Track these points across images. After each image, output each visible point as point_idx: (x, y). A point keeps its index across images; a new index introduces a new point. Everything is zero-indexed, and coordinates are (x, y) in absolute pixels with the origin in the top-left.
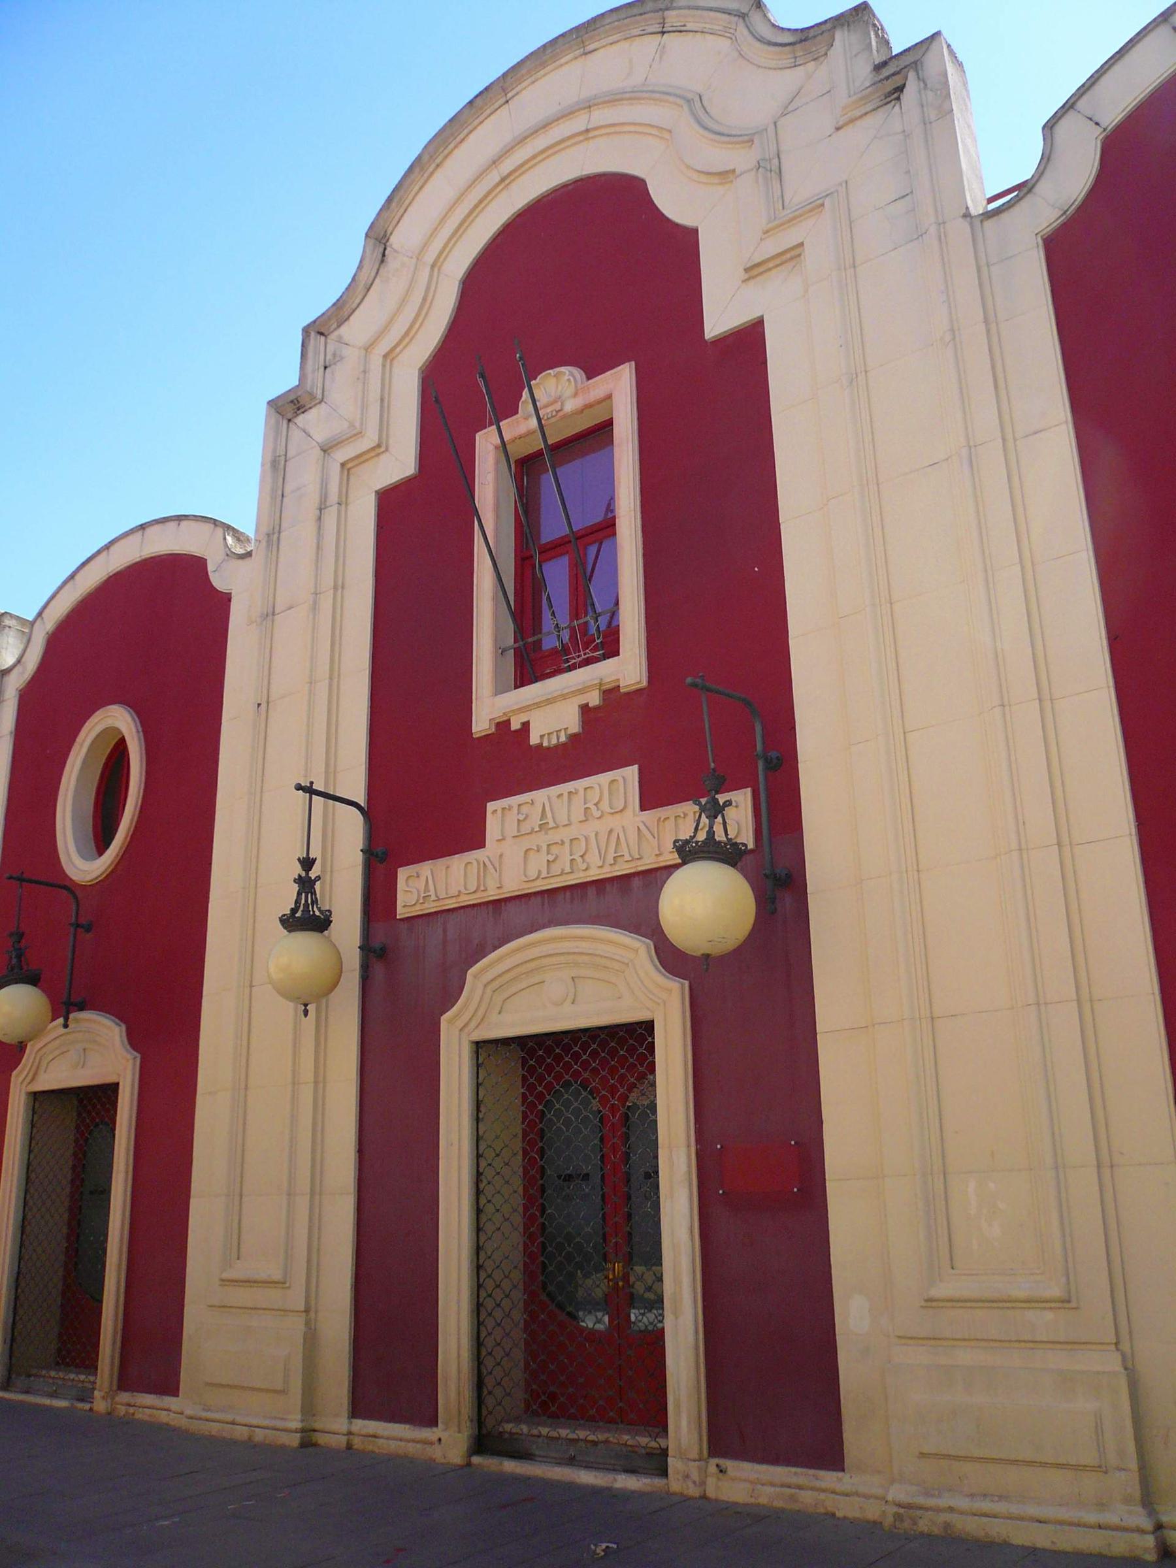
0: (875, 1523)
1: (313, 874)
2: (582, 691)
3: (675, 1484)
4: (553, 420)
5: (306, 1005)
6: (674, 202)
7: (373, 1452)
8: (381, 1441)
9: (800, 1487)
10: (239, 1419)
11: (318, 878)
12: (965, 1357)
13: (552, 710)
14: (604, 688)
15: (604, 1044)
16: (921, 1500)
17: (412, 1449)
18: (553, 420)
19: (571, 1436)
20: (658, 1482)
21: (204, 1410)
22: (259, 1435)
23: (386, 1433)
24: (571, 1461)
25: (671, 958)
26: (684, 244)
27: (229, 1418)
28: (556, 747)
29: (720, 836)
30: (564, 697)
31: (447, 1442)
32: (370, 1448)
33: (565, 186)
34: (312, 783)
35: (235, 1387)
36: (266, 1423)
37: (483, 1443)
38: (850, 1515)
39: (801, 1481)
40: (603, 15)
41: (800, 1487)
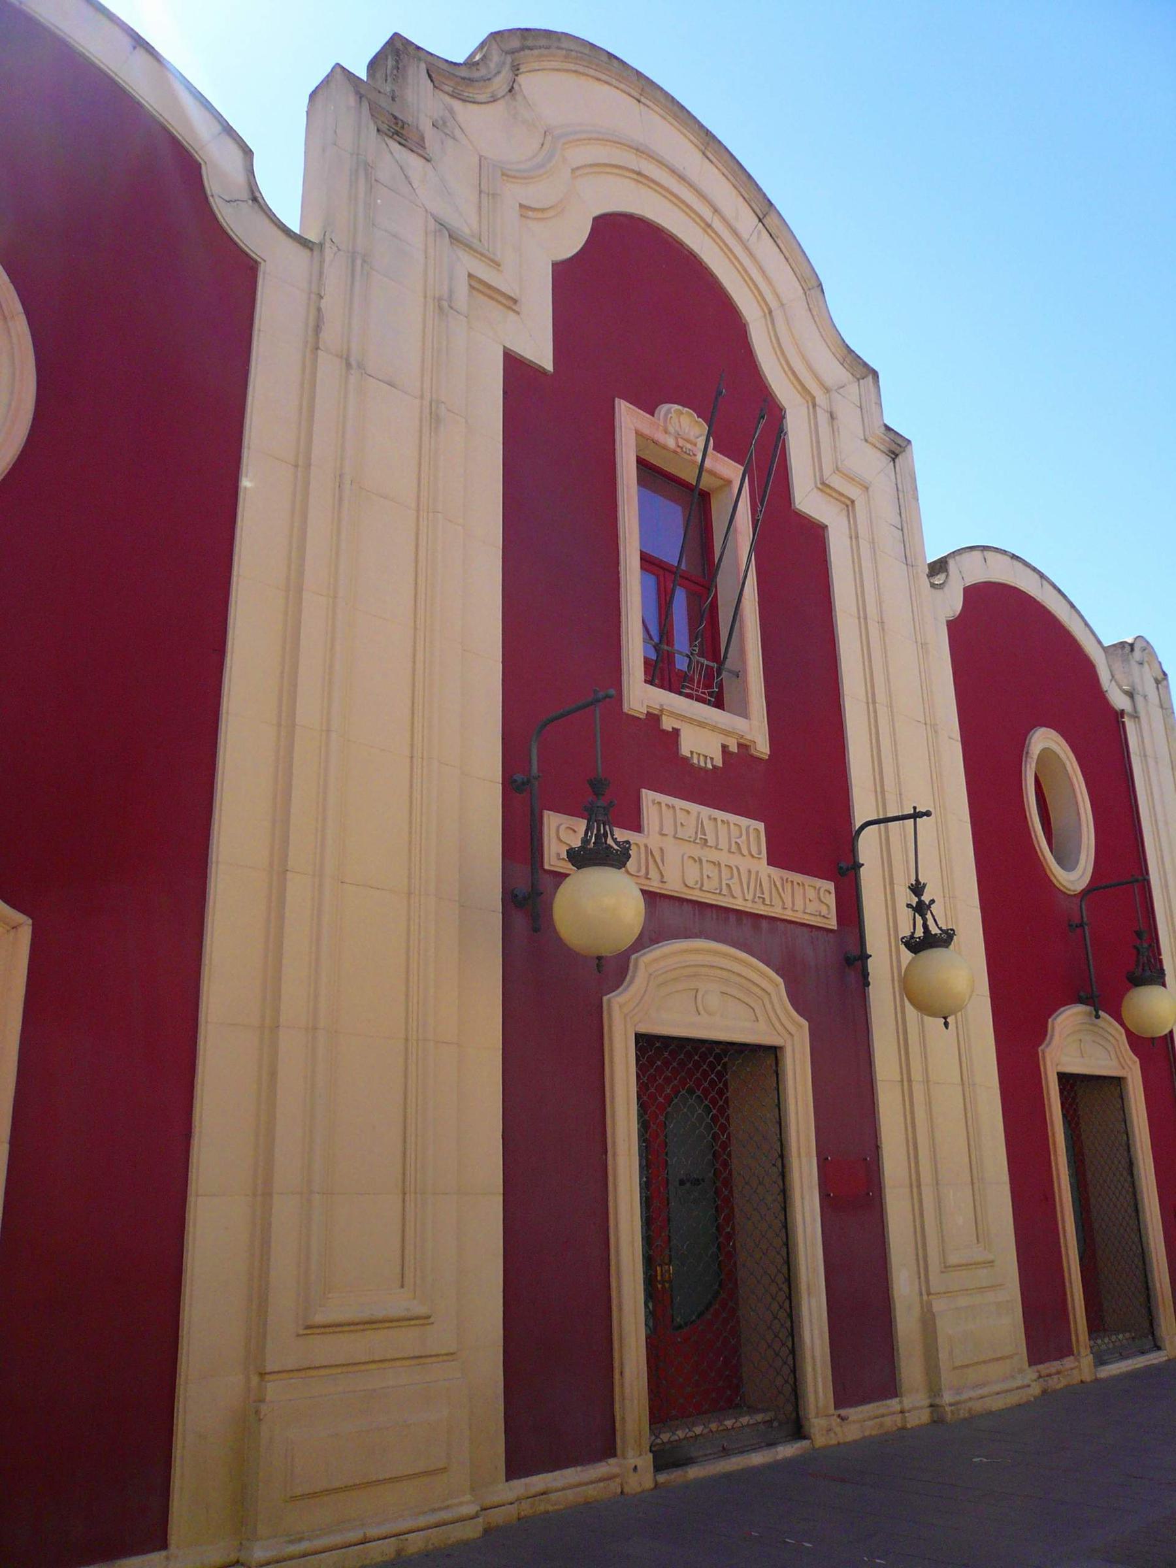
0: (899, 1429)
1: (926, 898)
2: (726, 733)
3: (820, 1440)
4: (686, 456)
5: (945, 1018)
6: (571, 239)
7: (547, 1512)
8: (553, 1496)
9: (883, 1416)
10: (373, 1532)
11: (933, 901)
12: (963, 1302)
13: (705, 733)
14: (742, 741)
15: (704, 1057)
16: (958, 1398)
17: (591, 1492)
18: (686, 456)
19: (751, 1422)
20: (787, 1451)
21: (291, 1542)
22: (415, 1544)
23: (559, 1484)
24: (725, 1452)
25: (1141, 1044)
26: (566, 275)
27: (354, 1536)
28: (700, 768)
29: (934, 930)
30: (714, 728)
31: (632, 1469)
32: (542, 1508)
33: (681, 244)
34: (915, 808)
35: (356, 1487)
36: (422, 1521)
37: (665, 1459)
38: (855, 1437)
39: (882, 1411)
40: (661, 89)
41: (883, 1416)
